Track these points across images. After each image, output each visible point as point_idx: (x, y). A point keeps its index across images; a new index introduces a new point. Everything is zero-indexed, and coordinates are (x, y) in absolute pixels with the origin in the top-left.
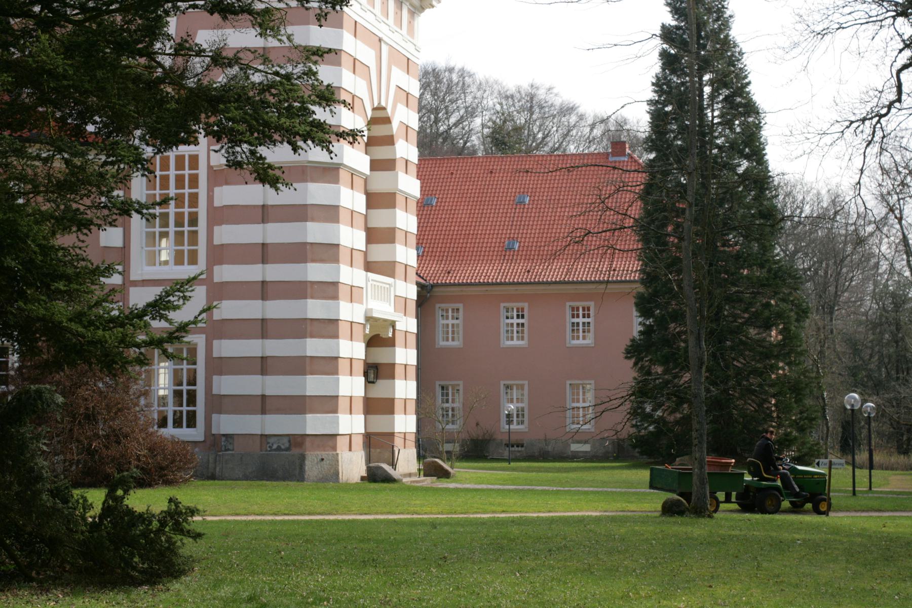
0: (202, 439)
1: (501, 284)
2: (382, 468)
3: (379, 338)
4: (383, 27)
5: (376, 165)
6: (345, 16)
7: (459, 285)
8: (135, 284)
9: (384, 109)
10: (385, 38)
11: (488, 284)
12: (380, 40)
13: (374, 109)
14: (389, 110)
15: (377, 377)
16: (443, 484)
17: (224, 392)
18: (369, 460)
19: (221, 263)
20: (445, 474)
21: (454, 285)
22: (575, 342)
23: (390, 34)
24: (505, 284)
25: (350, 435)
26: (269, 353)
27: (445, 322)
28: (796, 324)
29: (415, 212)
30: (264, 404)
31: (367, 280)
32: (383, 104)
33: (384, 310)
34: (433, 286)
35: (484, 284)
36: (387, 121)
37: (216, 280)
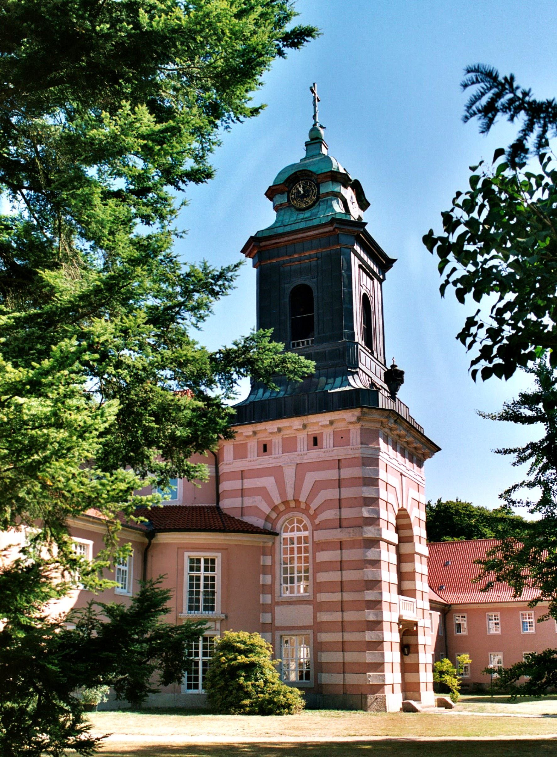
0: (313, 686)
1: (485, 603)
2: (410, 703)
3: (408, 630)
4: (402, 467)
5: (400, 540)
6: (380, 461)
7: (464, 604)
8: (278, 604)
9: (405, 510)
10: (404, 473)
11: (479, 603)
12: (401, 474)
13: (399, 510)
14: (408, 511)
15: (409, 652)
16: (449, 712)
17: (323, 660)
18: (405, 698)
19: (321, 592)
20: (448, 706)
21: (462, 604)
22: (526, 631)
23: (407, 471)
24: (487, 603)
25: (393, 685)
27: (531, 620)
28: (111, 237)
29: (426, 565)
30: (344, 668)
31: (399, 600)
32: (405, 507)
33: (409, 616)
34: (451, 605)
35: (477, 603)
36: (408, 516)
37: (318, 600)
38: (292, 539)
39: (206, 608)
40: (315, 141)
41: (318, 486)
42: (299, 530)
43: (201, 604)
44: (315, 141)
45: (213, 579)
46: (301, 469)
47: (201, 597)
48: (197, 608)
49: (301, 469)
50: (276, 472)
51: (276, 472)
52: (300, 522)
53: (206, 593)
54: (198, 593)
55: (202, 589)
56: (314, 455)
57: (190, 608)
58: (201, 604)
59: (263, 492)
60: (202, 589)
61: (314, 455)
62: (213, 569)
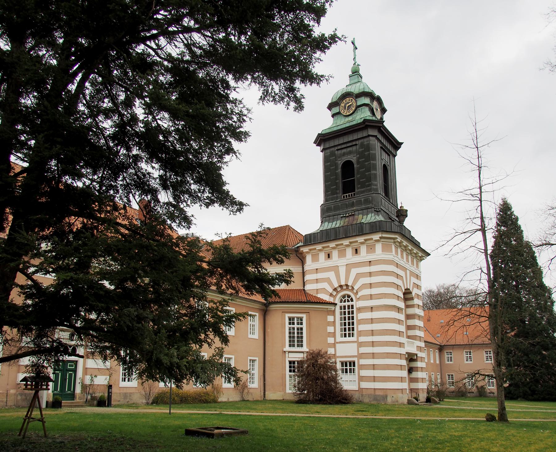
39: (298, 346)
40: (355, 73)
42: (348, 301)
43: (296, 343)
44: (355, 73)
46: (349, 267)
47: (296, 339)
48: (294, 346)
49: (349, 267)
51: (335, 269)
52: (349, 296)
53: (298, 337)
54: (294, 337)
55: (296, 335)
56: (357, 259)
57: (290, 346)
58: (296, 343)
59: (328, 280)
60: (296, 335)
61: (357, 259)
62: (302, 324)
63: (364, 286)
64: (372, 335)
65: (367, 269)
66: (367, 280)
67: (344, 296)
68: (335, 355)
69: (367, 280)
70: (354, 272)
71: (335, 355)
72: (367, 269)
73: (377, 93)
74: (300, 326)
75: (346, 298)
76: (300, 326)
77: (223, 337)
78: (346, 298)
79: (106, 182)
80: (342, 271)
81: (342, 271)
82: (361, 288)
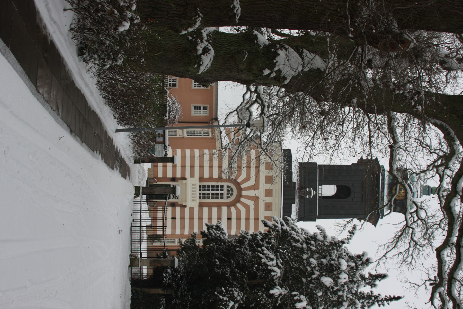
26: (198, 165)
38: (222, 190)
41: (247, 207)
42: (228, 194)
43: (219, 192)
45: (222, 198)
46: (256, 199)
49: (256, 199)
50: (256, 187)
51: (256, 187)
52: (232, 194)
58: (219, 192)
59: (248, 178)
63: (239, 212)
64: (193, 219)
65: (252, 216)
66: (243, 216)
67: (232, 190)
68: (163, 235)
69: (243, 216)
70: (251, 203)
71: (163, 235)
72: (252, 216)
73: (354, 237)
74: (202, 108)
75: (230, 192)
76: (202, 108)
77: (378, 277)
78: (230, 192)
79: (104, 49)
80: (251, 193)
81: (251, 193)
82: (237, 209)
